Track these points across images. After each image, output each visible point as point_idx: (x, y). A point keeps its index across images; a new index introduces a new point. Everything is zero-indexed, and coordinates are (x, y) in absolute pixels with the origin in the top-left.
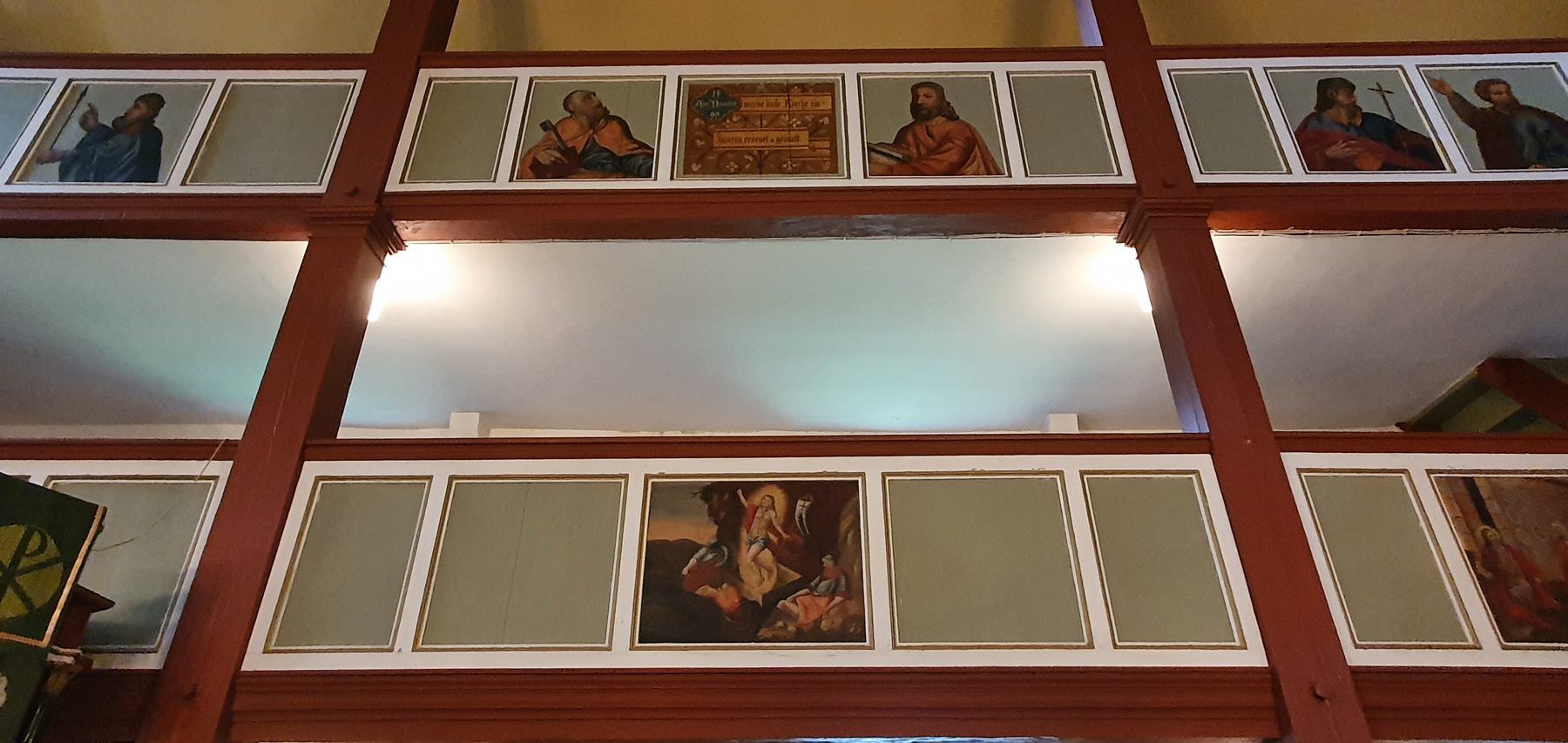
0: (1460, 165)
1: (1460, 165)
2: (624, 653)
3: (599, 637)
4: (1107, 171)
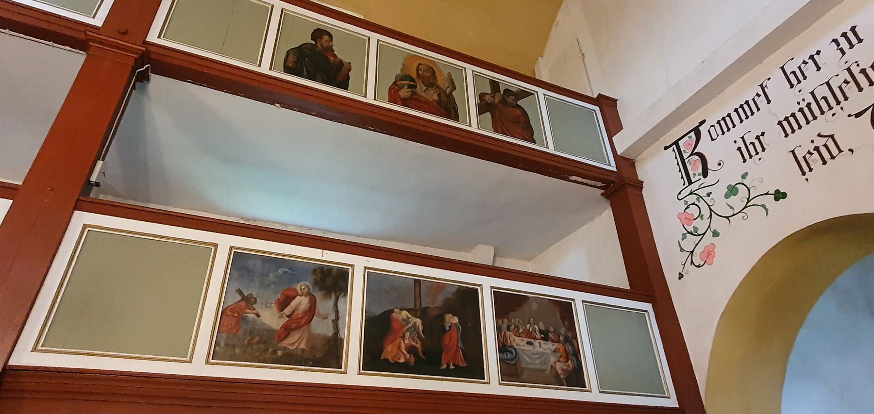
0: (473, 122)
1: (473, 122)
2: (199, 365)
3: (184, 353)
4: (253, 62)
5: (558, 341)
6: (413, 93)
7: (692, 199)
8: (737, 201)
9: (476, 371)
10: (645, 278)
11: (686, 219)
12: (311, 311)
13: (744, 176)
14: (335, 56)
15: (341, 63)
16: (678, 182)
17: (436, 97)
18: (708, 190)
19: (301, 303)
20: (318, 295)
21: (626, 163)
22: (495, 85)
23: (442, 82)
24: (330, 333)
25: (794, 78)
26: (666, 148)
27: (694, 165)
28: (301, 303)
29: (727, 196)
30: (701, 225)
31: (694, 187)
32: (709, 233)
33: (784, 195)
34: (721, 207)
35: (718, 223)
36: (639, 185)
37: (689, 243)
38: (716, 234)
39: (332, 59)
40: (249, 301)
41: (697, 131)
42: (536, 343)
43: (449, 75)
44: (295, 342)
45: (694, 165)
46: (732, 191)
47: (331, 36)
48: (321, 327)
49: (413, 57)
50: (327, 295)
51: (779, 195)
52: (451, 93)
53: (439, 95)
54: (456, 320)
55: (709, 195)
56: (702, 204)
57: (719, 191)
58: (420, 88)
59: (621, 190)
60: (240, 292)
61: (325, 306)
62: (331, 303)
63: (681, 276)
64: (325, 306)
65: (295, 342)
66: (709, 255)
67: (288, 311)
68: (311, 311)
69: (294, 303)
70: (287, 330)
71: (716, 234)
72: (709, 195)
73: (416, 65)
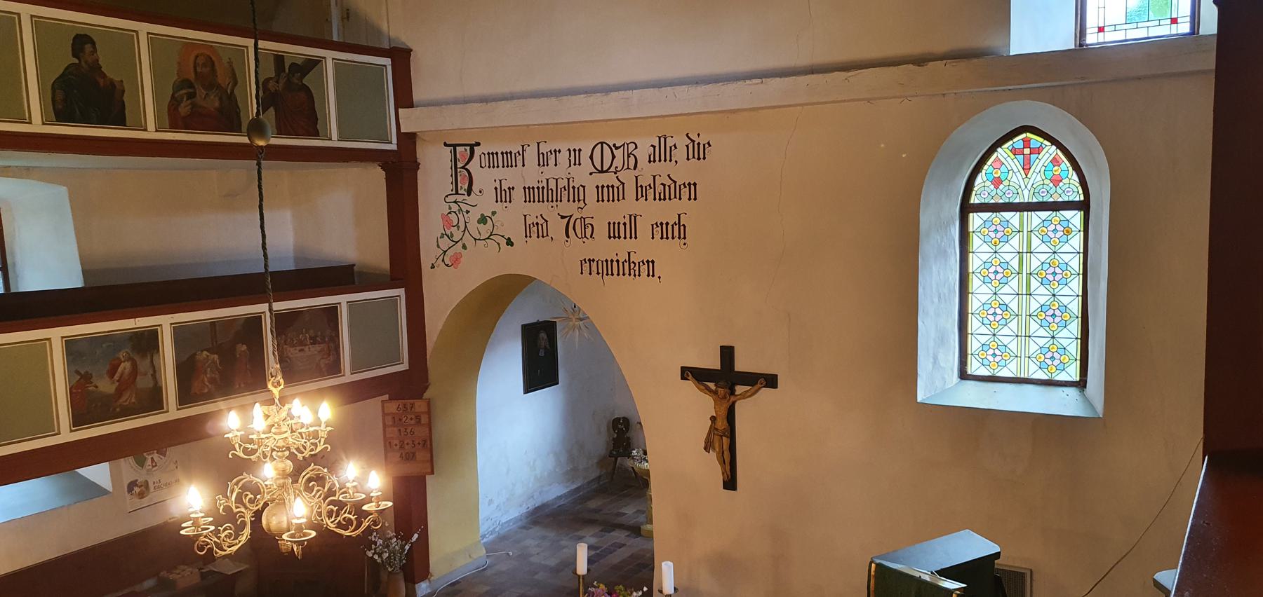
3: (53, 430)
5: (323, 342)
6: (194, 105)
7: (455, 207)
8: (485, 230)
9: (36, 21)
10: (404, 267)
11: (445, 218)
12: (135, 371)
13: (494, 213)
14: (104, 76)
15: (112, 83)
16: (449, 188)
17: (217, 104)
18: (468, 208)
19: (125, 367)
20: (137, 358)
21: (408, 140)
22: (279, 59)
23: (223, 79)
24: (151, 385)
25: (543, 160)
26: (446, 145)
27: (463, 182)
28: (125, 367)
29: (479, 222)
30: (457, 235)
31: (459, 198)
32: (460, 244)
33: (512, 244)
34: (473, 226)
35: (468, 240)
36: (416, 166)
37: (445, 243)
38: (464, 247)
39: (101, 81)
40: (86, 378)
41: (472, 147)
42: (306, 349)
43: (230, 63)
44: (128, 399)
45: (463, 182)
46: (483, 220)
47: (93, 43)
48: (143, 383)
49: (190, 45)
50: (144, 356)
51: (509, 243)
52: (232, 91)
53: (221, 99)
54: (244, 347)
55: (468, 212)
56: (461, 216)
57: (475, 215)
58: (201, 92)
59: (401, 169)
60: (78, 372)
61: (144, 365)
62: (148, 360)
63: (433, 267)
64: (144, 365)
65: (128, 399)
66: (456, 260)
67: (116, 377)
68: (135, 371)
69: (120, 370)
70: (119, 392)
71: (464, 247)
72: (468, 212)
73: (192, 58)
